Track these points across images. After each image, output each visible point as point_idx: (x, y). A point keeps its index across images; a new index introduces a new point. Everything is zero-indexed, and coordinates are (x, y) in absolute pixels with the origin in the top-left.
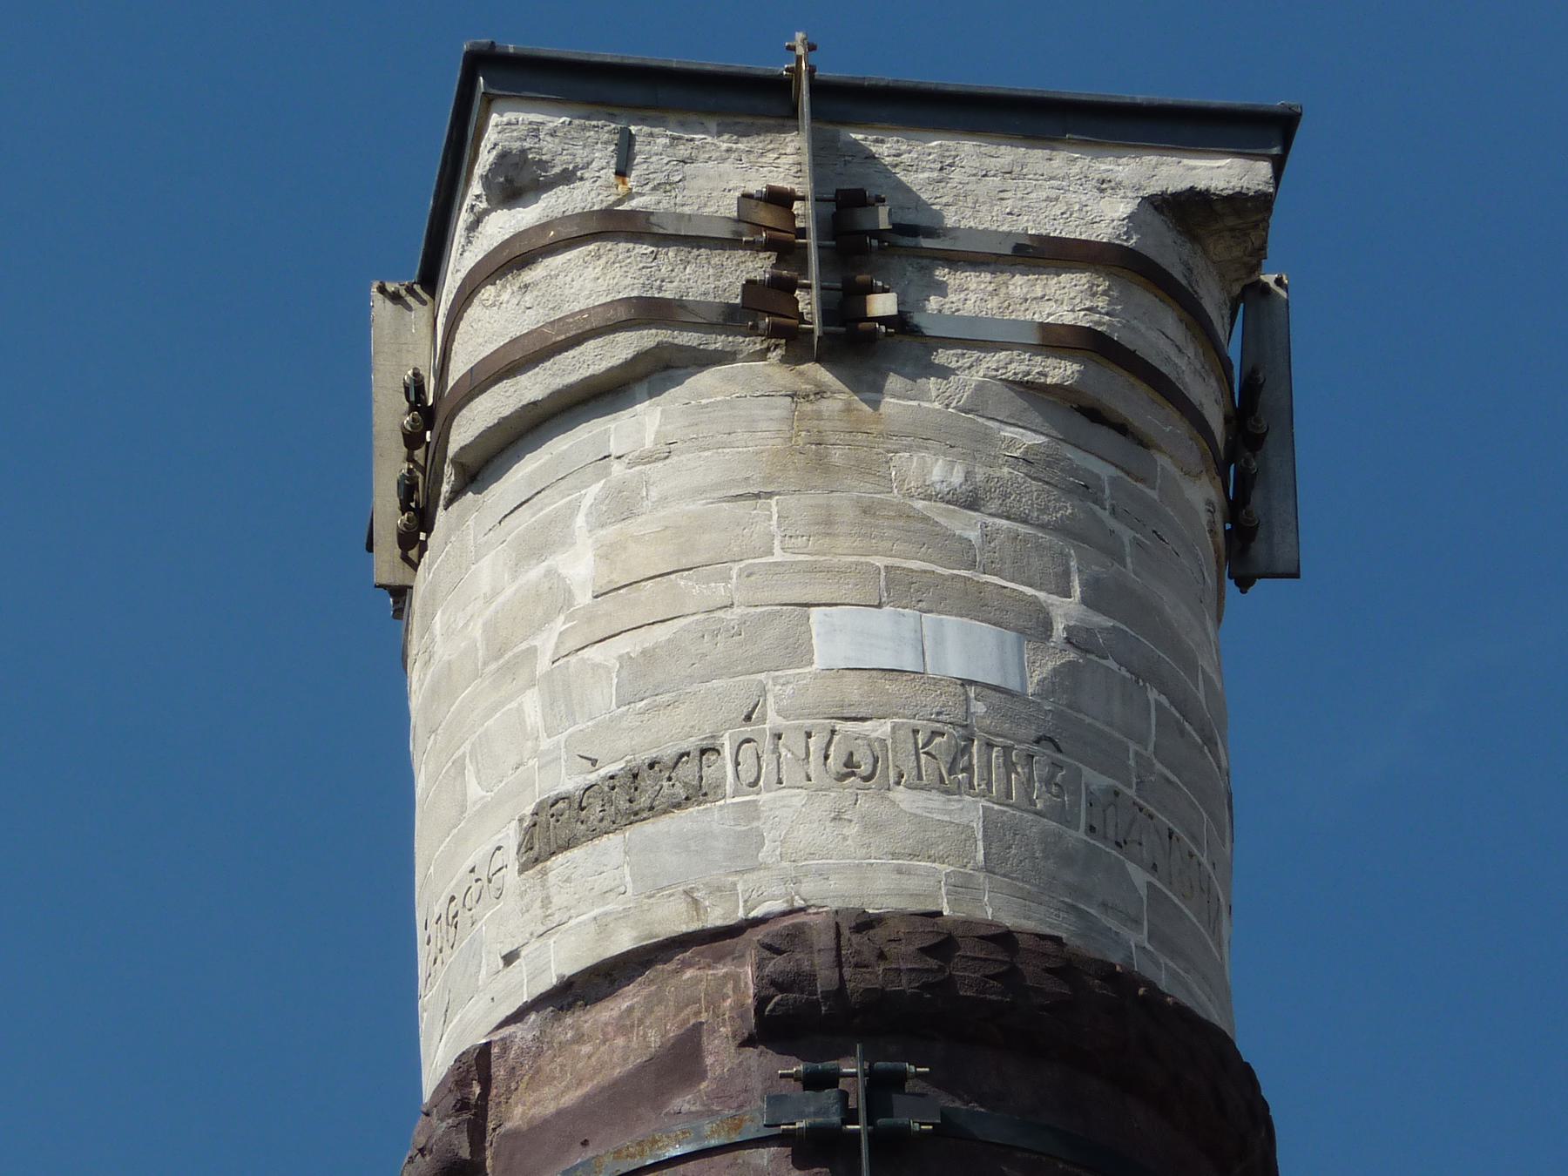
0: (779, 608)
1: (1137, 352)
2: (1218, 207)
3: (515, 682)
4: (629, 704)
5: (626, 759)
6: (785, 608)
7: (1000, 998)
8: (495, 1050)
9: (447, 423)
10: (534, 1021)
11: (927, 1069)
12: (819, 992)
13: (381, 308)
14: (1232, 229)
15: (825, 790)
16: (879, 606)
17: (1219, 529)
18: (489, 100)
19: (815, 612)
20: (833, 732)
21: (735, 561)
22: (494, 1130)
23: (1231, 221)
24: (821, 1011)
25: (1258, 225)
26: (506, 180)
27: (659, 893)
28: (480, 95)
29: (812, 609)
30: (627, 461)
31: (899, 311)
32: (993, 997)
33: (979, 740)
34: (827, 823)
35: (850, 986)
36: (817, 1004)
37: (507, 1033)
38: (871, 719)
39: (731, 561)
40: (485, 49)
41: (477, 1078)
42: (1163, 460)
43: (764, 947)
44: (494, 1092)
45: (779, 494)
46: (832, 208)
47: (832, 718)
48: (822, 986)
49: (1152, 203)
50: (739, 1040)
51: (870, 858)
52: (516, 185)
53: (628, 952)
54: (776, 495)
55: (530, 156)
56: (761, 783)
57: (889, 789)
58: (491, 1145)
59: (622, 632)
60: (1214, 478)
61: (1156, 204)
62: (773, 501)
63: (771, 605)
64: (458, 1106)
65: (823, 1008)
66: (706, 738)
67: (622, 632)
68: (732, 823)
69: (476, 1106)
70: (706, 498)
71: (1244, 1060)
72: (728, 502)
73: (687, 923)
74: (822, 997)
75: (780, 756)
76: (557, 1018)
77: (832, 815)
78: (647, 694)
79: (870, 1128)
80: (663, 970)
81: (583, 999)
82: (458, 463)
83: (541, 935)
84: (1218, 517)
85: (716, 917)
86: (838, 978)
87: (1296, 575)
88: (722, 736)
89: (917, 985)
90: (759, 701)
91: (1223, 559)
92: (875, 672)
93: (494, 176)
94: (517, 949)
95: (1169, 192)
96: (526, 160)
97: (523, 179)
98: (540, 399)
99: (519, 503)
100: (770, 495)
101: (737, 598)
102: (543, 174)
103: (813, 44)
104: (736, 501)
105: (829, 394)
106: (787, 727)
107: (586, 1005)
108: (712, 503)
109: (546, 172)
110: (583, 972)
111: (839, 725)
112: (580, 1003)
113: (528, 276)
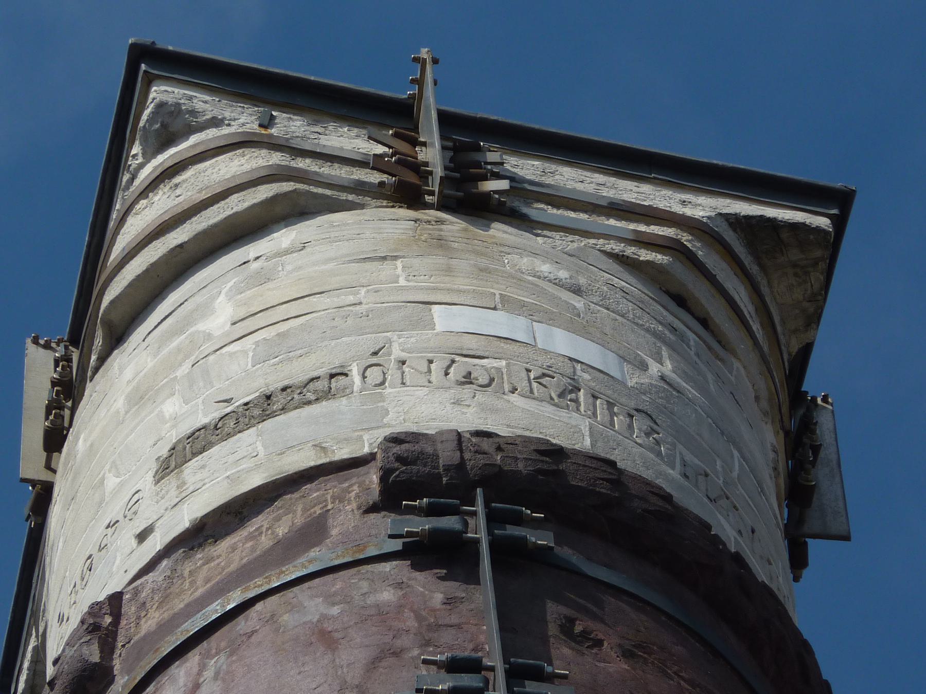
0: (403, 304)
1: (717, 277)
2: (785, 235)
3: (154, 404)
4: (264, 362)
5: (261, 390)
6: (409, 304)
7: (609, 492)
8: (127, 597)
9: (97, 302)
10: (166, 566)
11: (543, 515)
12: (441, 466)
13: (31, 348)
14: (795, 265)
15: (445, 388)
16: (495, 309)
17: (781, 467)
18: (149, 81)
19: (435, 308)
20: (453, 361)
21: (363, 286)
22: (123, 646)
23: (794, 255)
24: (442, 481)
25: (817, 264)
26: (162, 125)
27: (288, 450)
28: (142, 71)
29: (433, 306)
30: (265, 258)
31: (511, 187)
32: (603, 491)
33: (584, 389)
34: (448, 405)
35: (469, 465)
36: (439, 477)
37: (140, 583)
38: (487, 358)
39: (361, 286)
40: (148, 43)
41: (109, 612)
42: (737, 364)
43: (389, 442)
44: (123, 622)
45: (403, 257)
46: (451, 154)
47: (453, 354)
48: (444, 461)
49: (727, 220)
50: (364, 508)
51: (487, 425)
52: (171, 130)
53: (259, 487)
54: (401, 258)
55: (183, 108)
56: (387, 384)
57: (504, 394)
58: (120, 655)
59: (259, 329)
60: (778, 432)
61: (731, 220)
62: (399, 263)
63: (393, 302)
64: (90, 629)
65: (444, 479)
66: (335, 367)
67: (259, 329)
68: (359, 405)
69: (107, 629)
70: (338, 261)
71: (824, 678)
72: (358, 262)
73: (315, 461)
74: (444, 470)
75: (403, 372)
76: (186, 557)
77: (452, 401)
78: (282, 352)
79: (490, 537)
80: (291, 499)
81: (213, 537)
82: (108, 326)
83: (175, 505)
84: (782, 456)
85: (343, 453)
86: (459, 456)
87: (847, 538)
88: (350, 365)
89: (532, 469)
90: (385, 346)
91: (783, 497)
92: (491, 338)
93: (151, 125)
94: (151, 524)
95: (741, 214)
96: (180, 111)
97: (177, 125)
98: (186, 240)
99: (163, 317)
100: (396, 258)
101: (364, 301)
102: (194, 120)
103: (435, 58)
104: (365, 262)
105: (448, 223)
106: (409, 357)
107: (216, 542)
108: (343, 264)
109: (197, 118)
110: (214, 511)
111: (457, 358)
112: (209, 541)
113: (177, 180)
